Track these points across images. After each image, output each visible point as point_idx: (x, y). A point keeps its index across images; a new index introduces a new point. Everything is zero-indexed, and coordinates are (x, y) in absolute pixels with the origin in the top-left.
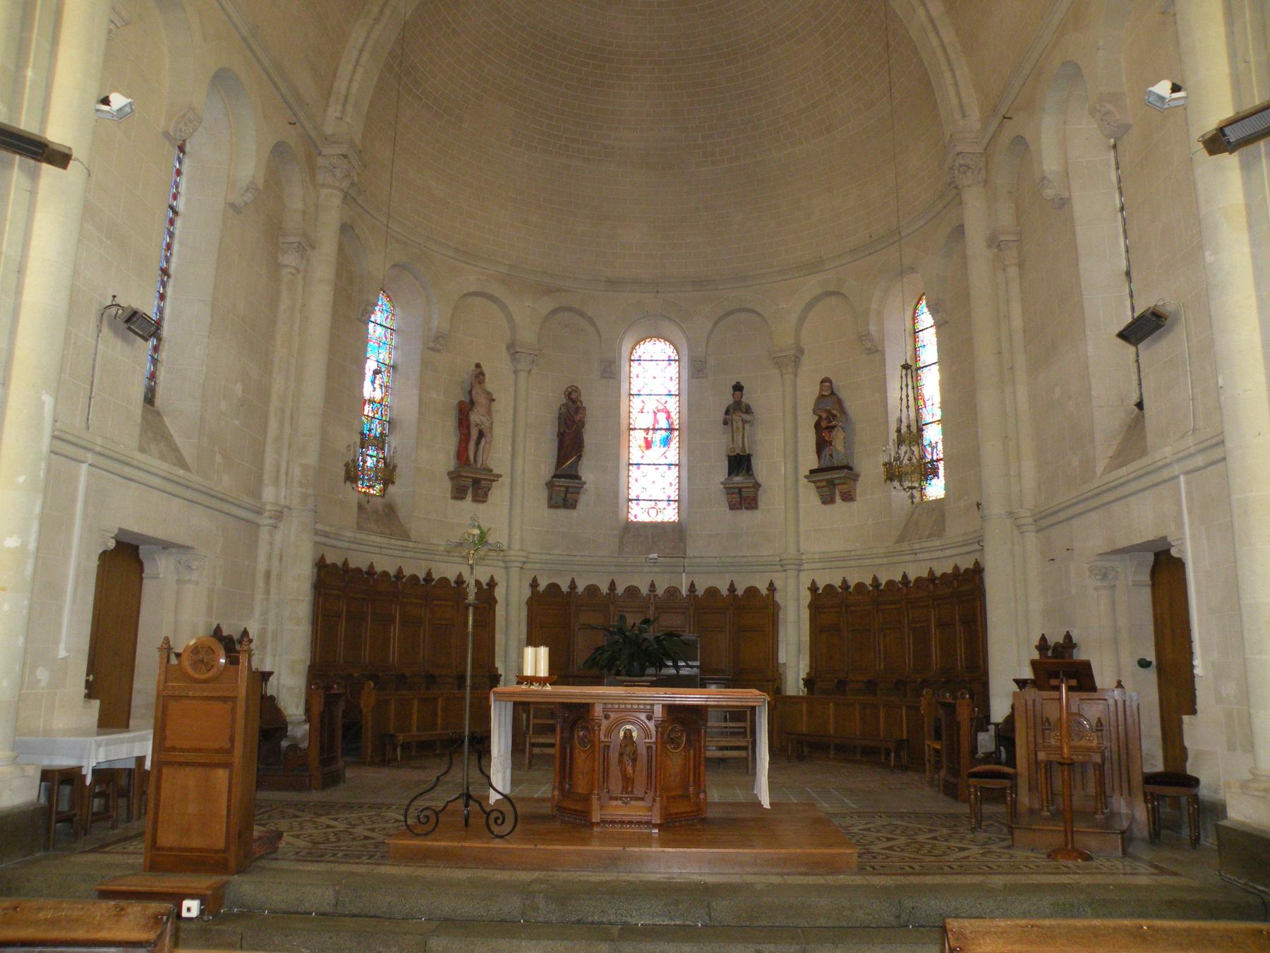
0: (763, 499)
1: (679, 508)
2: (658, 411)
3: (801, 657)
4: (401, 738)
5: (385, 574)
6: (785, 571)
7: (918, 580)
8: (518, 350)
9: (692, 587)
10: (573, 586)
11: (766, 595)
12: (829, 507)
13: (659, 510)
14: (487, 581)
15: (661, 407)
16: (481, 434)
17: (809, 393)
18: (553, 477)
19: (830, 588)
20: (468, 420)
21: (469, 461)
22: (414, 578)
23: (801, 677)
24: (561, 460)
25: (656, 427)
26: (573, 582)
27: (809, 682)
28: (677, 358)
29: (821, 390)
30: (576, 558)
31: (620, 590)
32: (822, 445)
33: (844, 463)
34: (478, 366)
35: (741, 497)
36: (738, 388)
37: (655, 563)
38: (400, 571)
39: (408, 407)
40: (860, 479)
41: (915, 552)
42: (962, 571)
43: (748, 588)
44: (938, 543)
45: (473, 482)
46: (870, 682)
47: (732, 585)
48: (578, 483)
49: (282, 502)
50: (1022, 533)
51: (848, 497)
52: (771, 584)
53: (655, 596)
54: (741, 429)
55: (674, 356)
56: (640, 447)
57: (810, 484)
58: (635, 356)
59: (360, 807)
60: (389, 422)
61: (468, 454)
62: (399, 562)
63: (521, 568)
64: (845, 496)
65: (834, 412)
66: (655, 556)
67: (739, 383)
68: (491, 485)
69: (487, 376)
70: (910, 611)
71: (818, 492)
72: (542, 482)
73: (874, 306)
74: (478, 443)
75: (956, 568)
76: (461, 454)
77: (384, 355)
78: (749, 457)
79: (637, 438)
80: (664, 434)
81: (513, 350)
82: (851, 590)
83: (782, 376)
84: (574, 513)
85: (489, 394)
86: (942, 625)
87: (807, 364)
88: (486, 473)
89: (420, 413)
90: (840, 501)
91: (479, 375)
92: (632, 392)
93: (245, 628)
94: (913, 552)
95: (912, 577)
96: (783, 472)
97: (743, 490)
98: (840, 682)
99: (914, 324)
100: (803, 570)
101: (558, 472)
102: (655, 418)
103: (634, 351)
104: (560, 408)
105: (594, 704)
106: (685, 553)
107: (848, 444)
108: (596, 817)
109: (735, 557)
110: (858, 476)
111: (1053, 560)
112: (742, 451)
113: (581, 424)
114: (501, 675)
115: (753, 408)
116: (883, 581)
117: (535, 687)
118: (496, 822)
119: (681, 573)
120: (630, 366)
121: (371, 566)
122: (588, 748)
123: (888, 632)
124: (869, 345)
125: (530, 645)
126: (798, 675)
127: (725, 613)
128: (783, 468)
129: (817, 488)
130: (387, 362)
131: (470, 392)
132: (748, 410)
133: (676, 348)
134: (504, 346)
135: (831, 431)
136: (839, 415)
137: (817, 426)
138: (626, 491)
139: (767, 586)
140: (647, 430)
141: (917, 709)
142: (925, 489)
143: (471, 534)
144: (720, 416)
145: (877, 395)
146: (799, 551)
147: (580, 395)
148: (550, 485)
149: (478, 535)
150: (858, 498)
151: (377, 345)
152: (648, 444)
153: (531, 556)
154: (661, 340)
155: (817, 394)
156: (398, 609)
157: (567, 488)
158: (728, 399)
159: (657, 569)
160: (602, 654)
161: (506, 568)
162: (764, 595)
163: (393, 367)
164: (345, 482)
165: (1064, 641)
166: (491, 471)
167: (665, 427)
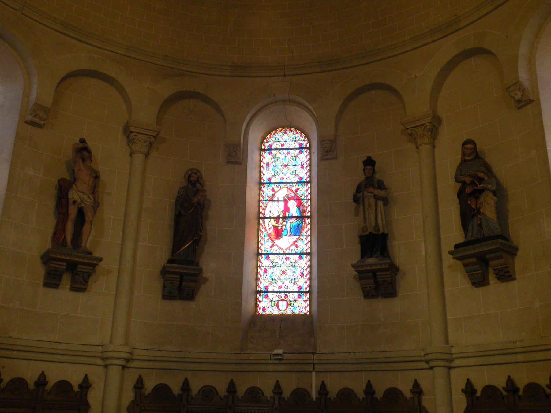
0: (403, 285)
1: (310, 299)
6: (431, 368)
8: (132, 129)
9: (323, 389)
10: (186, 387)
12: (480, 291)
13: (289, 303)
14: (36, 378)
15: (292, 195)
16: (81, 213)
19: (490, 389)
21: (66, 243)
23: (448, 245)
24: (177, 244)
25: (287, 215)
28: (308, 146)
29: (464, 154)
31: (241, 391)
36: (369, 162)
37: (280, 360)
43: (387, 390)
52: (416, 385)
61: (65, 236)
63: (124, 367)
65: (481, 175)
66: (280, 351)
67: (370, 158)
72: (158, 270)
73: (523, 50)
79: (268, 225)
82: (521, 393)
83: (417, 148)
84: (192, 305)
87: (444, 133)
90: (496, 280)
92: (262, 181)
96: (423, 253)
100: (454, 368)
115: (386, 183)
119: (311, 372)
124: (519, 96)
128: (423, 248)
129: (465, 265)
132: (381, 186)
133: (307, 136)
136: (486, 178)
137: (460, 194)
140: (277, 219)
146: (447, 342)
148: (164, 272)
154: (292, 129)
155: (459, 162)
157: (182, 275)
159: (282, 368)
161: (106, 366)
162: (361, 398)
166: (91, 254)
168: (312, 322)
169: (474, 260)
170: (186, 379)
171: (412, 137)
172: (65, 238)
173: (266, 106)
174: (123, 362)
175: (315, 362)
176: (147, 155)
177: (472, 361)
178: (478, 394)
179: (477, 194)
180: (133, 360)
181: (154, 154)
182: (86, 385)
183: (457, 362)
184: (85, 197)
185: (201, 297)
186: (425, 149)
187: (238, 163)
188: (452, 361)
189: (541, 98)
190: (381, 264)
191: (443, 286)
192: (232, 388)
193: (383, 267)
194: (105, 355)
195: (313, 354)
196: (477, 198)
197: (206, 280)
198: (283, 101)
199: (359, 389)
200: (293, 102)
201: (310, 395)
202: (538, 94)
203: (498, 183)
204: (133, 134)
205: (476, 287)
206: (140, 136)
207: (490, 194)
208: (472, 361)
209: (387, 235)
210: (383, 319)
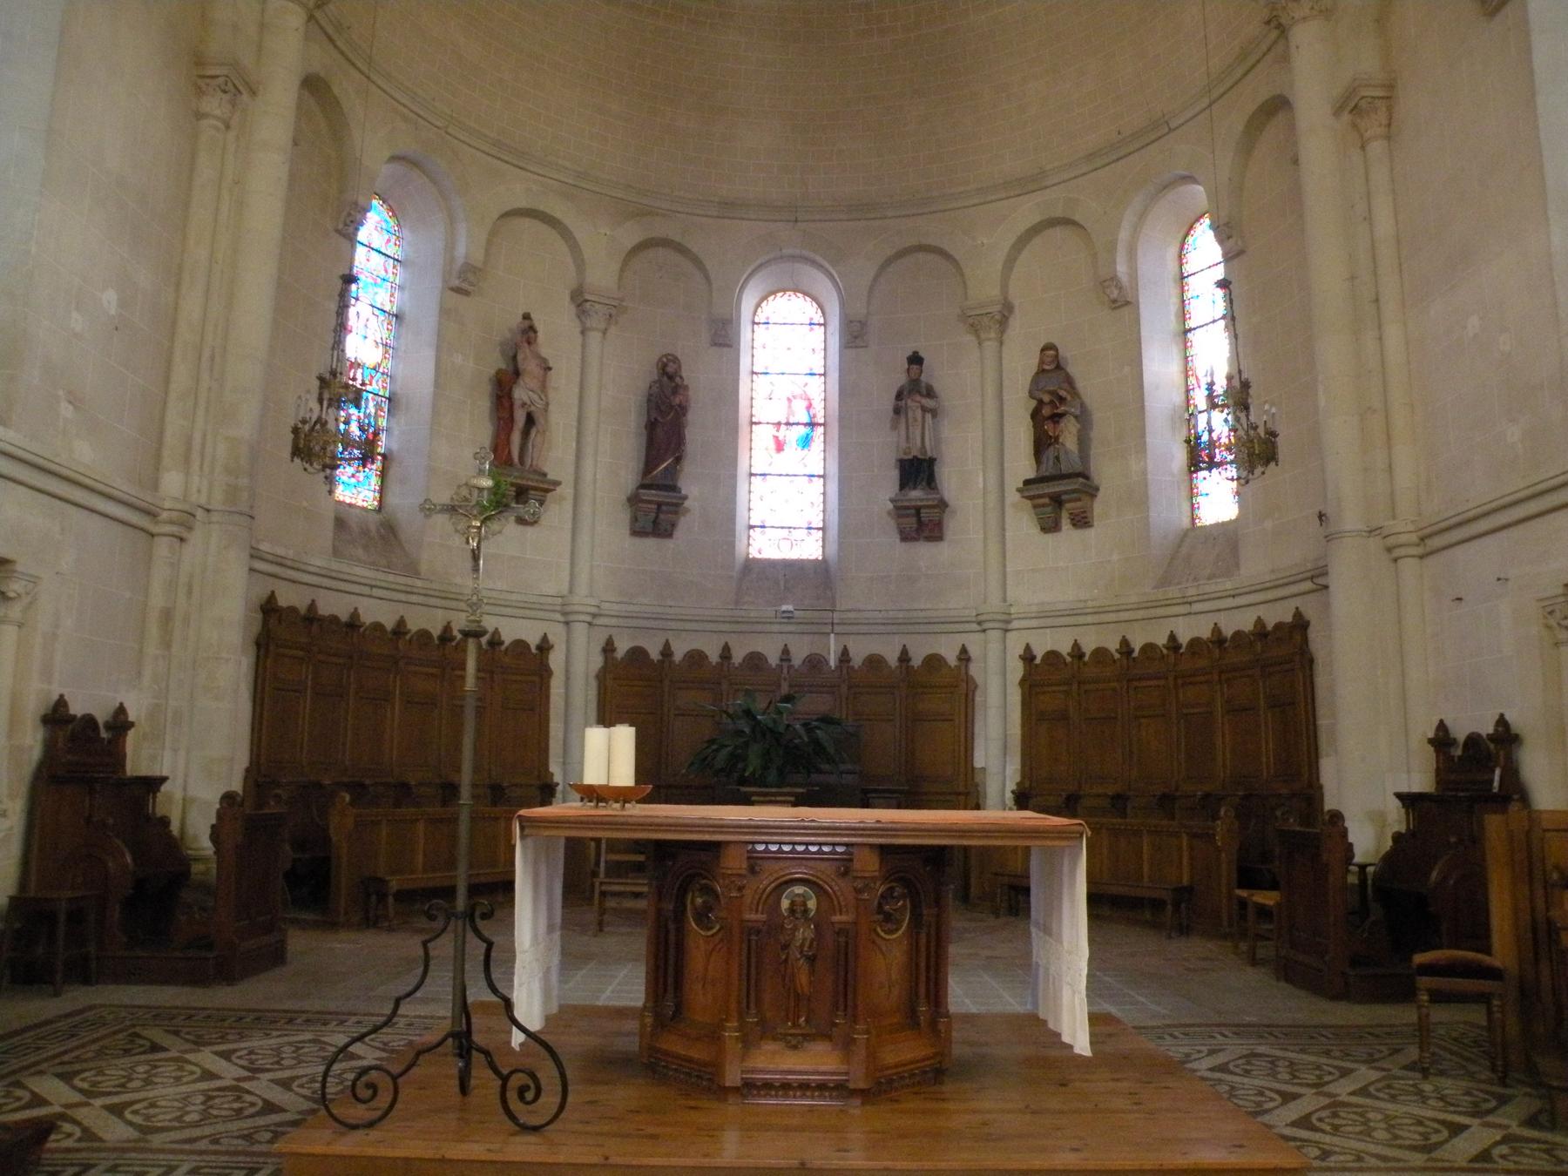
0: (952, 526)
2: (794, 397)
3: (1008, 759)
4: (394, 884)
5: (378, 626)
6: (984, 631)
7: (1195, 642)
8: (588, 297)
9: (845, 656)
12: (1049, 537)
13: (794, 543)
15: (798, 391)
16: (530, 421)
17: (1021, 366)
18: (638, 488)
19: (1052, 656)
20: (510, 397)
22: (424, 635)
24: (650, 463)
25: (791, 421)
26: (667, 645)
28: (822, 321)
29: (1042, 362)
30: (672, 611)
32: (1043, 443)
33: (1078, 468)
34: (527, 317)
35: (919, 521)
36: (916, 360)
37: (789, 618)
38: (401, 622)
39: (420, 374)
40: (1101, 494)
41: (1190, 599)
42: (1270, 627)
43: (927, 656)
44: (1229, 585)
45: (516, 492)
46: (1164, 796)
48: (675, 497)
49: (194, 498)
50: (1395, 560)
51: (1082, 521)
52: (964, 650)
53: (790, 667)
54: (920, 419)
55: (819, 318)
56: (767, 449)
57: (1024, 500)
58: (760, 318)
59: (290, 1021)
60: (390, 399)
62: (402, 610)
64: (1077, 519)
65: (1063, 393)
66: (790, 608)
68: (545, 497)
69: (541, 335)
71: (1037, 514)
73: (1124, 235)
74: (526, 433)
75: (1259, 622)
76: (500, 447)
77: (383, 298)
78: (931, 462)
79: (762, 437)
80: (803, 430)
81: (579, 300)
82: (1086, 658)
83: (980, 344)
84: (669, 544)
85: (545, 360)
87: (1016, 324)
88: (537, 477)
89: (437, 384)
91: (529, 331)
93: (121, 704)
94: (1185, 600)
95: (1184, 639)
96: (981, 486)
97: (922, 511)
98: (1069, 798)
99: (1181, 265)
101: (647, 482)
102: (790, 407)
103: (759, 310)
104: (650, 387)
105: (728, 843)
106: (834, 604)
107: (1084, 442)
108: (732, 1077)
110: (1097, 489)
111: (1460, 599)
112: (921, 454)
113: (682, 410)
114: (557, 784)
116: (1137, 645)
117: (613, 809)
118: (521, 1097)
119: (829, 634)
120: (753, 331)
121: (355, 614)
122: (714, 931)
125: (1435, 747)
126: (1004, 785)
127: (893, 694)
129: (1035, 507)
130: (387, 308)
131: (515, 357)
132: (930, 393)
133: (821, 306)
134: (567, 293)
135: (1058, 422)
136: (1069, 398)
137: (1035, 415)
138: (746, 513)
139: (958, 653)
141: (1209, 837)
142: (1198, 508)
143: (474, 487)
144: (888, 402)
145: (1127, 369)
146: (1005, 600)
147: (680, 367)
148: (634, 500)
149: (489, 489)
150: (1095, 523)
151: (372, 281)
152: (780, 446)
153: (605, 606)
155: (1035, 370)
156: (398, 683)
157: (659, 505)
158: (900, 379)
160: (717, 750)
161: (567, 623)
163: (397, 316)
164: (292, 461)
165: (1496, 730)
166: (545, 475)
167: (805, 422)
168: (827, 571)
169: (1046, 500)
170: (667, 641)
171: (975, 329)
172: (509, 452)
173: (768, 262)
174: (588, 618)
176: (605, 332)
177: (1034, 623)
178: (1038, 661)
179: (1056, 418)
180: (601, 615)
181: (613, 330)
182: (545, 647)
183: (1015, 624)
184: (535, 397)
185: (679, 532)
186: (991, 346)
187: (729, 346)
188: (1008, 622)
189: (1141, 300)
190: (928, 500)
191: (1004, 529)
192: (726, 653)
193: (930, 503)
194: (568, 609)
195: (832, 611)
196: (1056, 423)
197: (687, 510)
198: (794, 258)
200: (814, 263)
201: (827, 663)
202: (1137, 296)
203: (1082, 405)
204: (589, 303)
205: (1046, 533)
206: (597, 306)
207: (1072, 420)
208: (1034, 623)
209: (935, 460)
210: (924, 569)
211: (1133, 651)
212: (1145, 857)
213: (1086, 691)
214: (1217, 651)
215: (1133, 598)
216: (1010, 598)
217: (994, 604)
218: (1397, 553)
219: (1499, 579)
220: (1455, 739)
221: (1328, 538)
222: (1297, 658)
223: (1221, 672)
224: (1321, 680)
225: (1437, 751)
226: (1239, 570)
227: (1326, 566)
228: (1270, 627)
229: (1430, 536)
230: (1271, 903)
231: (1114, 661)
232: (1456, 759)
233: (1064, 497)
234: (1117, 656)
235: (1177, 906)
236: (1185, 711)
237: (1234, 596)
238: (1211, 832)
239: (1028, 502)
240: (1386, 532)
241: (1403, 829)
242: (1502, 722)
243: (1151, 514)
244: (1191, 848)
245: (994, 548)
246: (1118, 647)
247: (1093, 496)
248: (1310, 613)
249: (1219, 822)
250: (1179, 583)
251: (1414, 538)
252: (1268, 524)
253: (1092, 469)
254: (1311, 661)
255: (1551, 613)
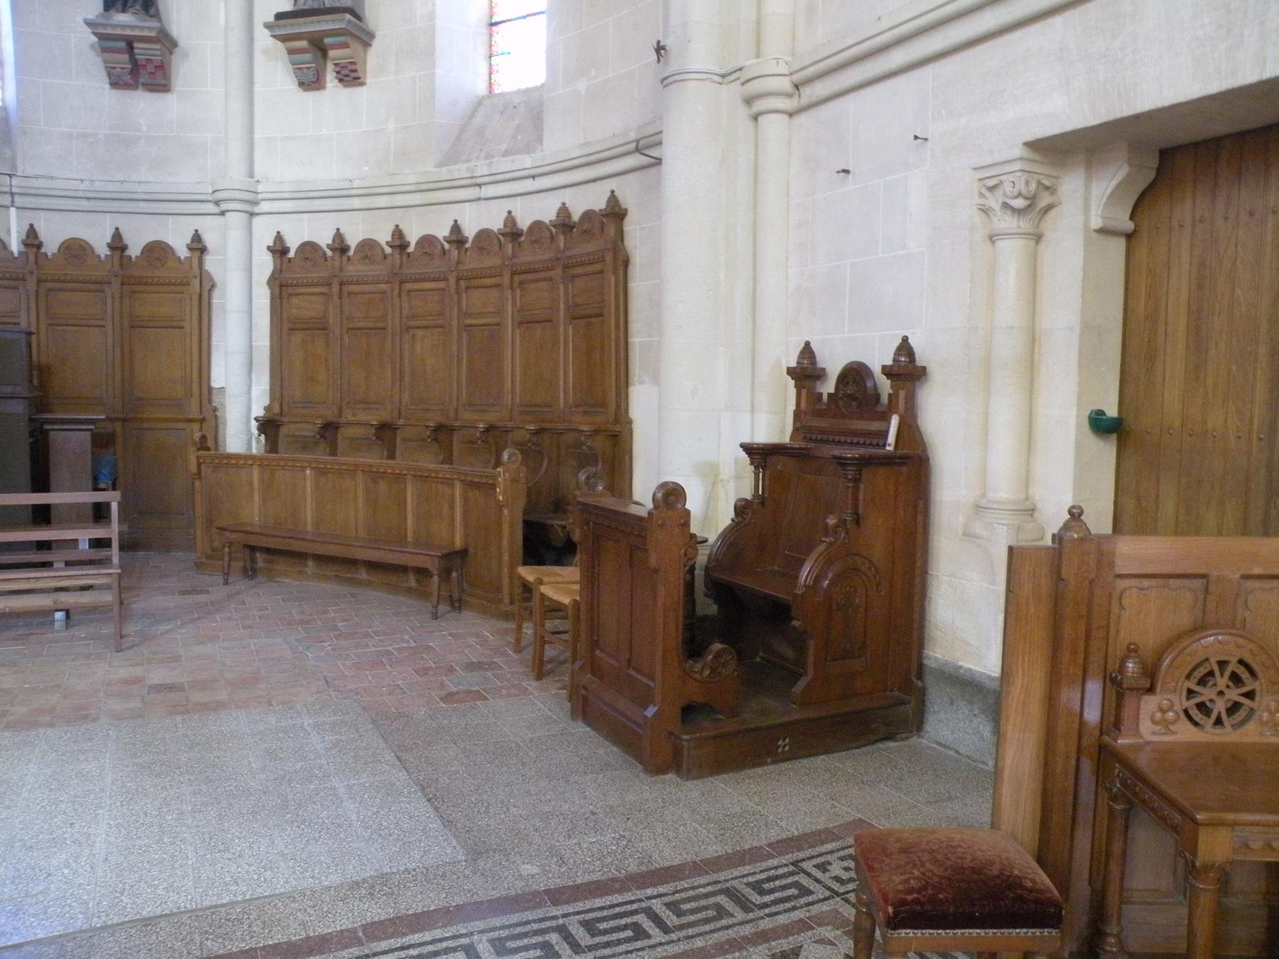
0: (182, 71)
7: (483, 235)
11: (186, 258)
12: (311, 96)
19: (308, 248)
27: (268, 426)
40: (376, 44)
41: (479, 181)
42: (576, 217)
44: (528, 163)
47: (117, 235)
50: (755, 118)
51: (351, 76)
52: (197, 237)
64: (346, 72)
70: (464, 295)
82: (351, 253)
86: (525, 322)
94: (474, 181)
95: (470, 231)
106: (14, 167)
109: (123, 182)
111: (846, 172)
119: (7, 207)
123: (420, 333)
125: (796, 381)
128: (222, 13)
129: (291, 52)
139: (188, 241)
146: (251, 175)
150: (368, 81)
169: (303, 44)
175: (15, 190)
183: (264, 207)
188: (255, 203)
199: (100, 242)
205: (306, 90)
210: (144, 128)
211: (408, 244)
212: (409, 507)
213: (349, 294)
214: (510, 246)
215: (410, 177)
216: (259, 171)
217: (235, 177)
218: (760, 105)
219: (916, 138)
220: (823, 370)
221: (665, 82)
222: (609, 257)
223: (513, 274)
224: (638, 287)
225: (799, 387)
226: (542, 144)
227: (661, 132)
228: (576, 217)
229: (809, 81)
230: (566, 600)
231: (385, 257)
232: (825, 397)
233: (327, 41)
234: (388, 250)
235: (445, 574)
236: (468, 321)
237: (533, 177)
238: (491, 482)
239: (280, 45)
240: (745, 75)
241: (748, 494)
242: (905, 348)
243: (438, 71)
244: (466, 500)
245: (237, 106)
246: (389, 239)
247: (367, 45)
248: (628, 199)
249: (500, 469)
250: (467, 161)
251: (785, 84)
252: (582, 85)
253: (366, 7)
254: (627, 263)
255: (992, 189)
